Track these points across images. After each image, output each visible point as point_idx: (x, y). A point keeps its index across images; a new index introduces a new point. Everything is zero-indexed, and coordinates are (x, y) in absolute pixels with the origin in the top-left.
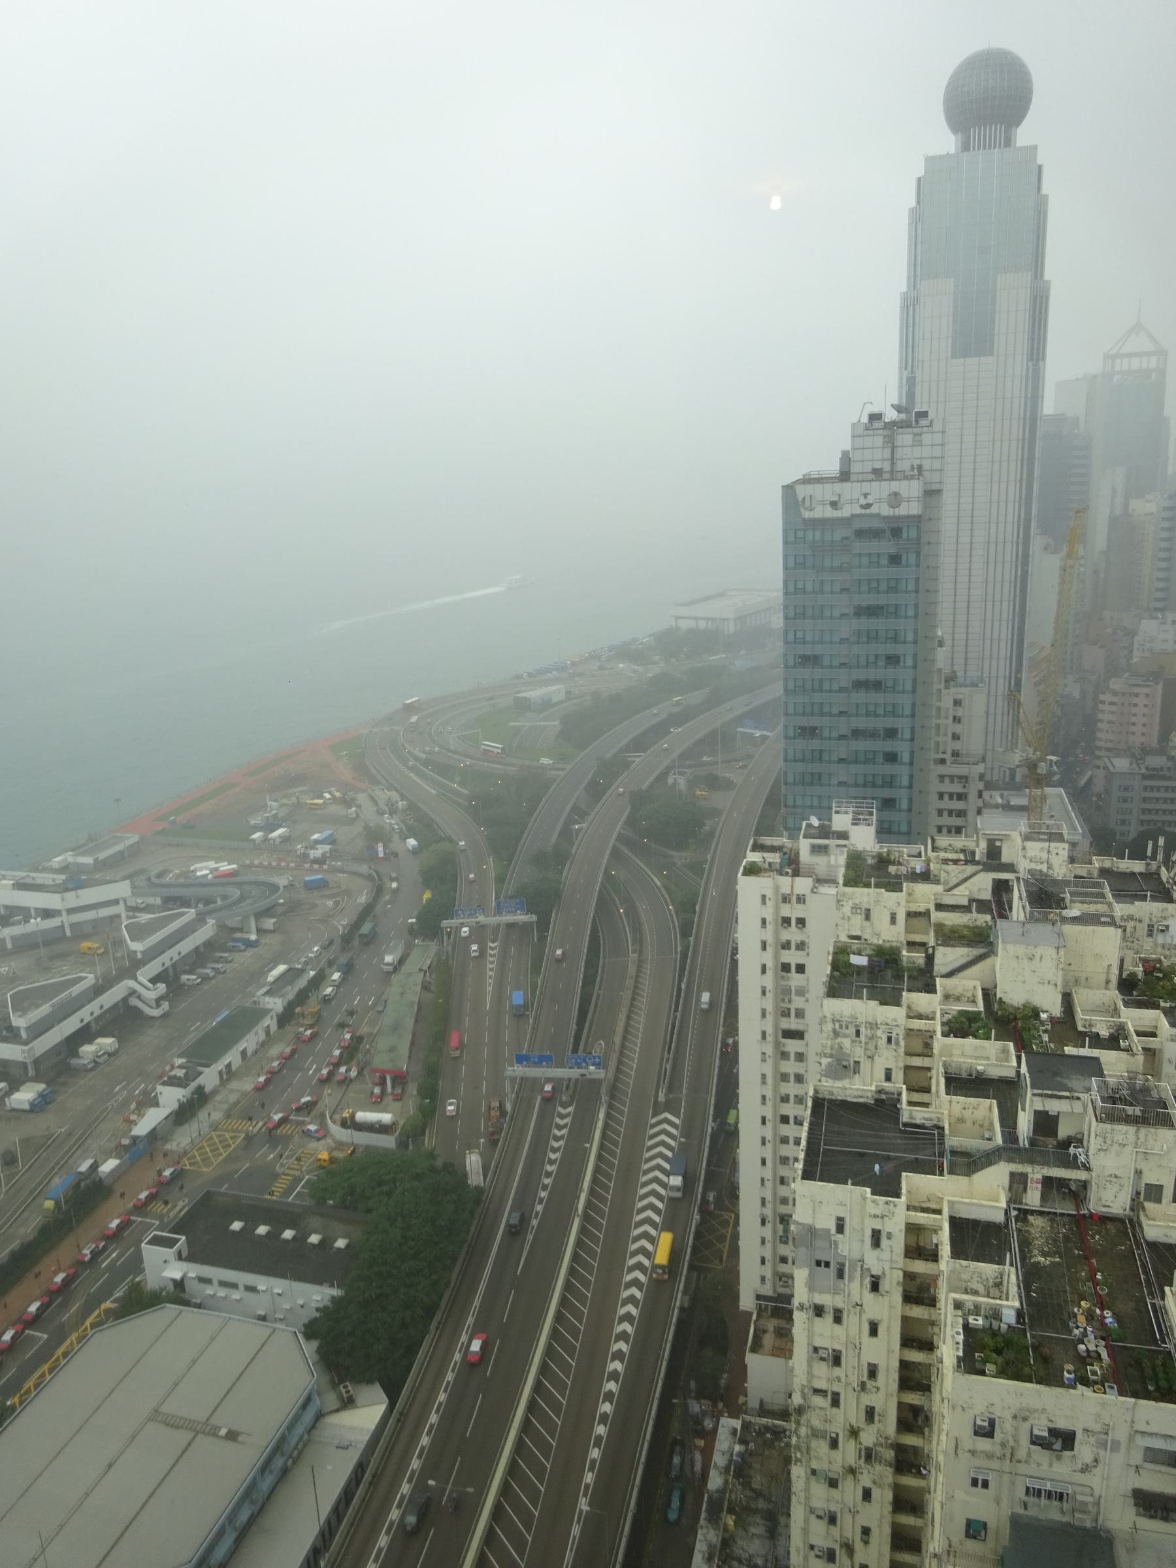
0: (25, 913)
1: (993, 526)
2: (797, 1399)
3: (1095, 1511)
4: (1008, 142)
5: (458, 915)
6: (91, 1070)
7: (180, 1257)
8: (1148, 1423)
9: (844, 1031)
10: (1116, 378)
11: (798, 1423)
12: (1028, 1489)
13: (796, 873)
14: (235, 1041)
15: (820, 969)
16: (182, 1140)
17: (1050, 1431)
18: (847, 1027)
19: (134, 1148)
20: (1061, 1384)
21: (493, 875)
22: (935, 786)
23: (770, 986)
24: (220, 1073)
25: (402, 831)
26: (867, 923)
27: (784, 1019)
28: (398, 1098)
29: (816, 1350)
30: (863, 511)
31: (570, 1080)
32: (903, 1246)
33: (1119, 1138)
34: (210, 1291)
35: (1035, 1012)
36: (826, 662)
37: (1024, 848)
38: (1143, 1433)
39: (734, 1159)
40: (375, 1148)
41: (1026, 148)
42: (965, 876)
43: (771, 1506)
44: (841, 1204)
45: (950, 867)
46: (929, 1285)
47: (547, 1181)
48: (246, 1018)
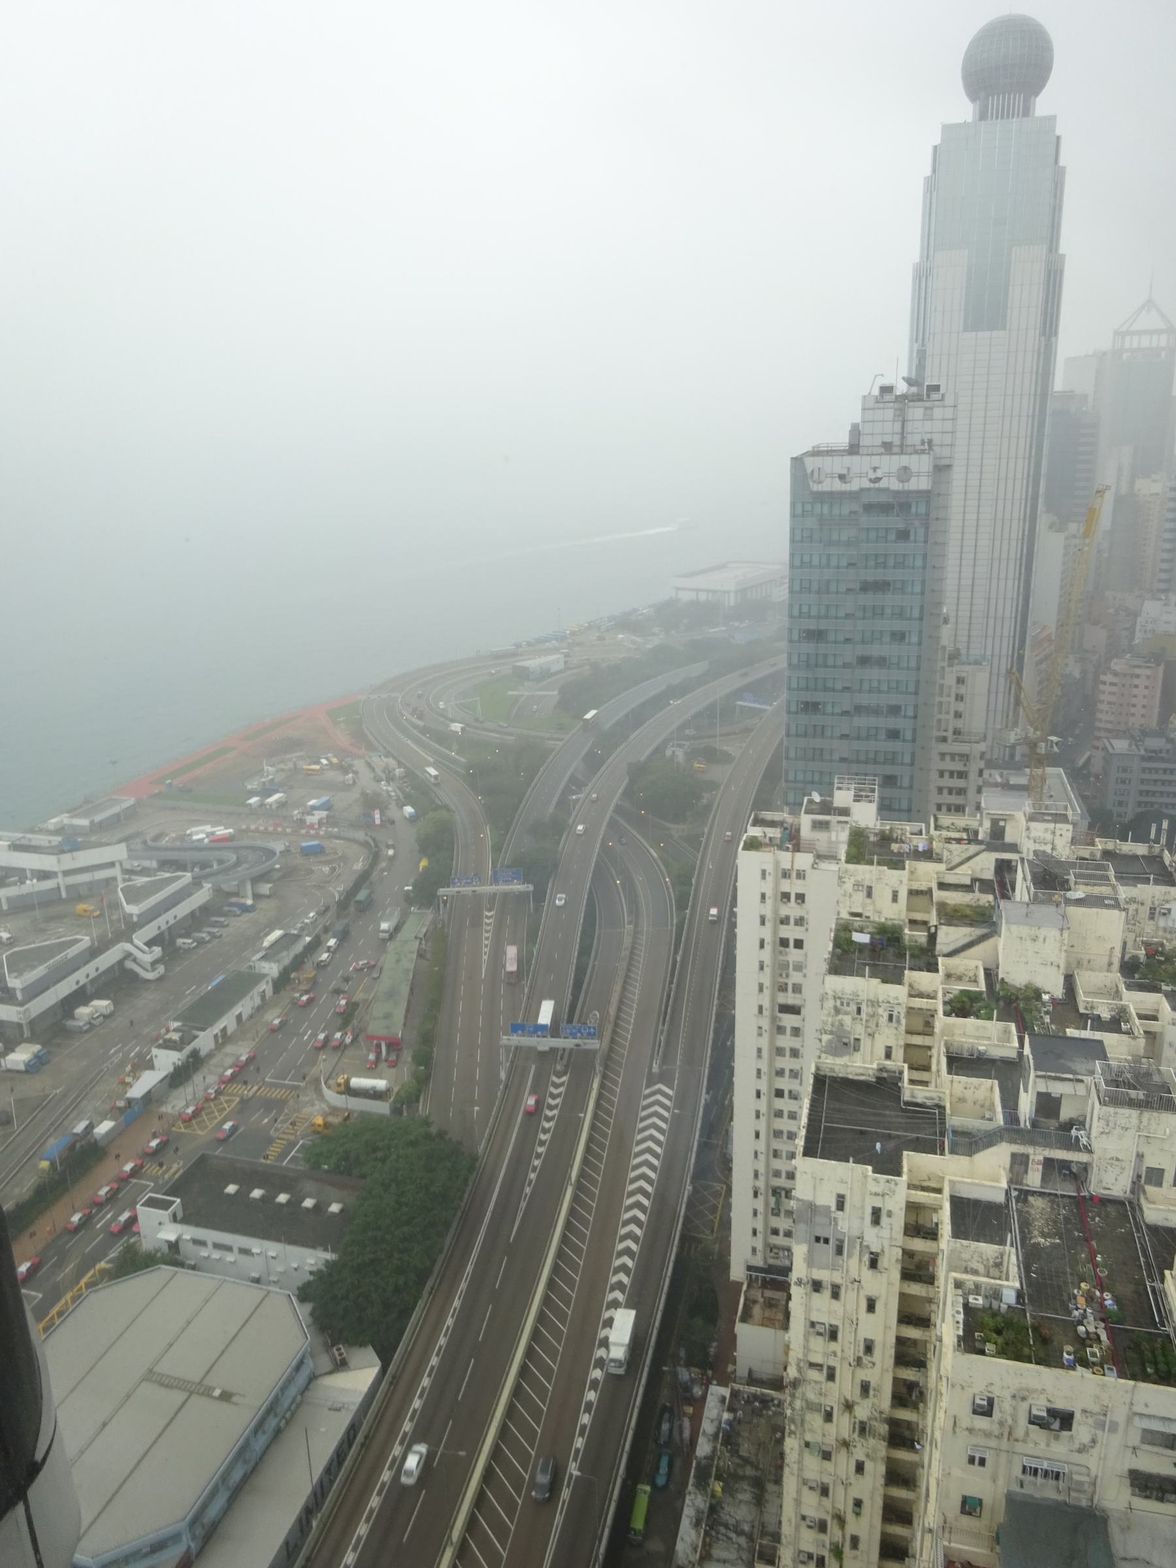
0: (21, 875)
1: (1000, 503)
2: (792, 1372)
3: (1090, 1490)
4: (1027, 111)
5: (454, 884)
6: (86, 1032)
7: (174, 1219)
8: (1146, 1405)
9: (845, 1008)
10: (1125, 356)
11: (793, 1396)
12: (1024, 1467)
13: (797, 849)
14: (231, 1004)
15: (820, 946)
16: (180, 1102)
17: (1049, 1411)
18: (848, 1005)
19: (129, 1111)
20: (1061, 1366)
21: (489, 843)
22: (937, 764)
23: (768, 962)
24: (216, 1036)
25: (398, 798)
26: (868, 901)
27: (781, 994)
28: (394, 1065)
29: (813, 1324)
30: (872, 485)
31: (564, 1050)
32: (903, 1224)
33: (1122, 1121)
34: (204, 1253)
35: (1038, 994)
36: (831, 637)
37: (1028, 829)
38: (1141, 1415)
39: (727, 1132)
40: (370, 1114)
41: (1045, 118)
42: (968, 855)
43: (758, 1474)
44: (842, 1181)
45: (954, 846)
46: (928, 1263)
47: (540, 1150)
48: (244, 982)
